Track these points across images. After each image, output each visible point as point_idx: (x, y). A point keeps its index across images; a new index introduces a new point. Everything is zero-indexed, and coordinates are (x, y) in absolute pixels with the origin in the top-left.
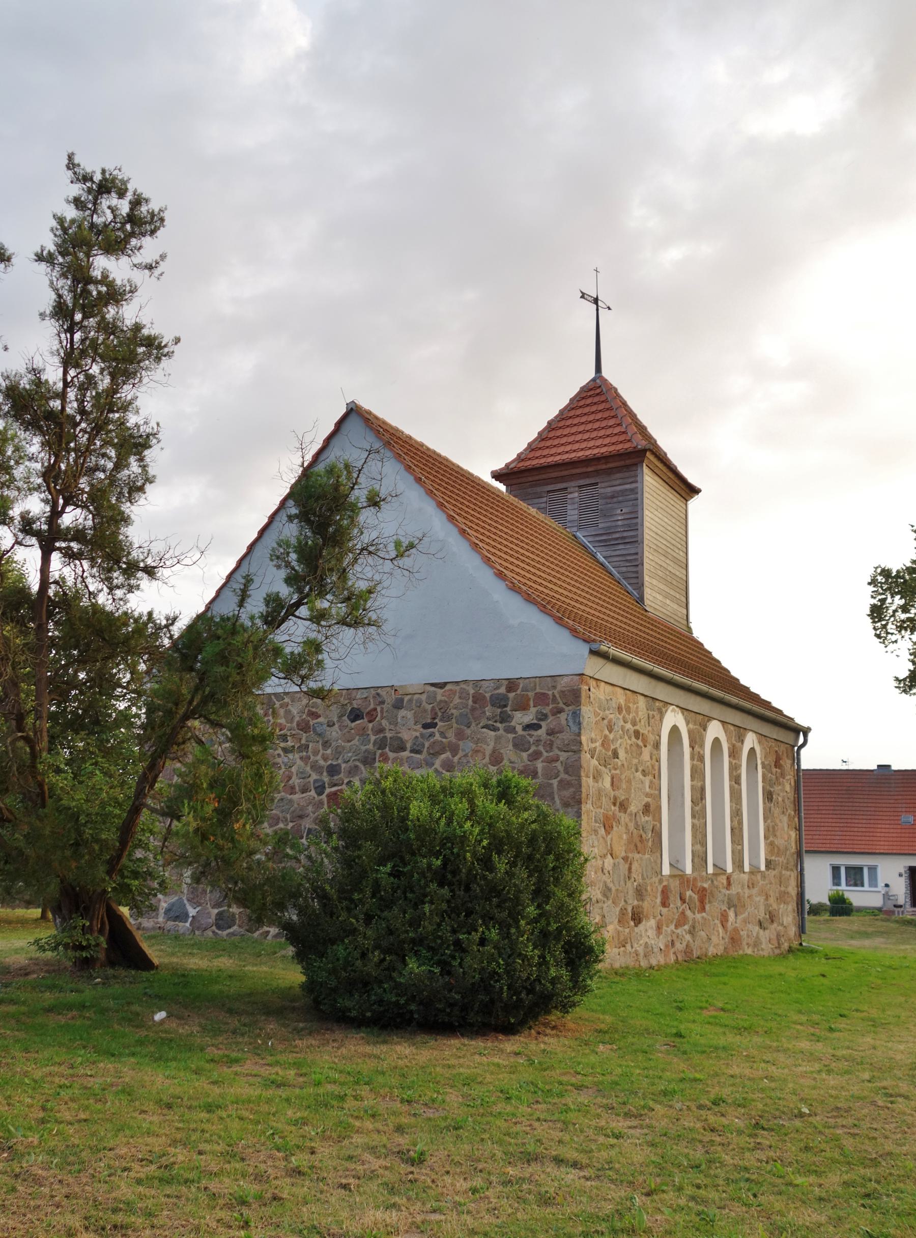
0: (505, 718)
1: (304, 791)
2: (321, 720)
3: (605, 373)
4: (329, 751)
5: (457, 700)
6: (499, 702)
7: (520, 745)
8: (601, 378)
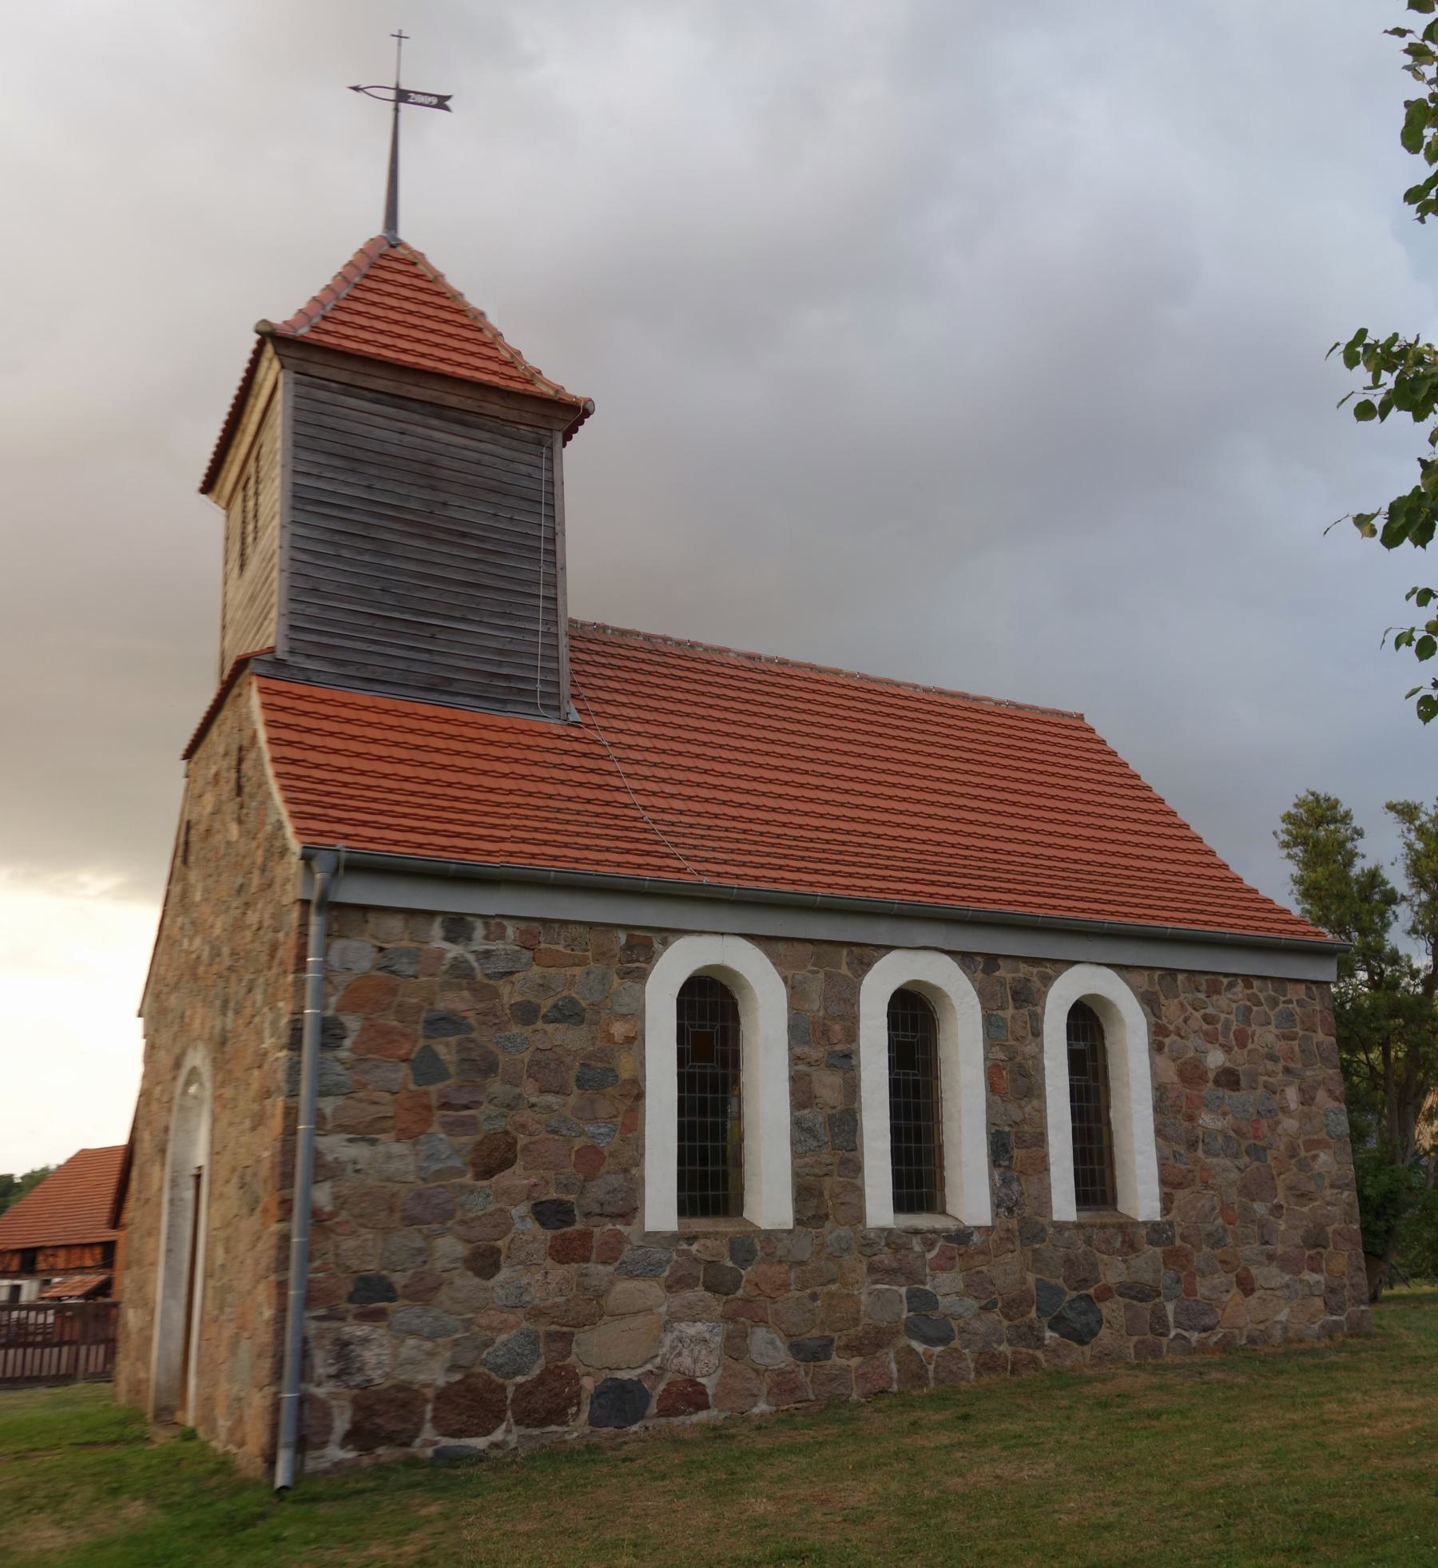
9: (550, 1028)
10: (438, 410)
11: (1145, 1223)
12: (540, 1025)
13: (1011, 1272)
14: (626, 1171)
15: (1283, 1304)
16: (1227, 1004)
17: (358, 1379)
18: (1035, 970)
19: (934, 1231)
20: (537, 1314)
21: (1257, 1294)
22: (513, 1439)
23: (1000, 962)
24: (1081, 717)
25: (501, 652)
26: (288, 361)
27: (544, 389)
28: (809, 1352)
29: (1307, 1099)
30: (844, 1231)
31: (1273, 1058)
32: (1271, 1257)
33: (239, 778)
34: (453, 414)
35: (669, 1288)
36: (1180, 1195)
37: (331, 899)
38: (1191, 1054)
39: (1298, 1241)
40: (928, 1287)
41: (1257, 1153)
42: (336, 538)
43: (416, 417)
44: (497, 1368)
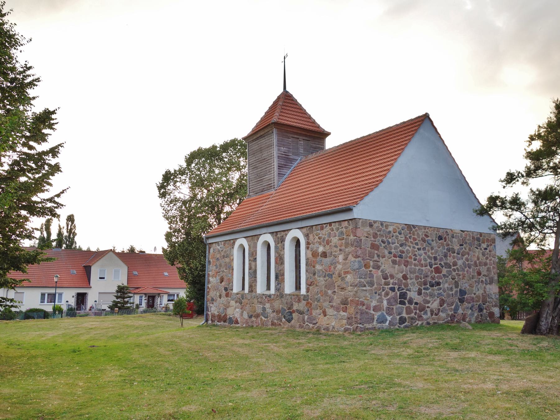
0: (480, 245)
1: (426, 266)
2: (429, 238)
3: (287, 89)
4: (433, 251)
5: (468, 238)
6: (478, 240)
7: (483, 254)
8: (287, 92)
13: (278, 305)
28: (250, 317)
30: (254, 294)
32: (332, 306)
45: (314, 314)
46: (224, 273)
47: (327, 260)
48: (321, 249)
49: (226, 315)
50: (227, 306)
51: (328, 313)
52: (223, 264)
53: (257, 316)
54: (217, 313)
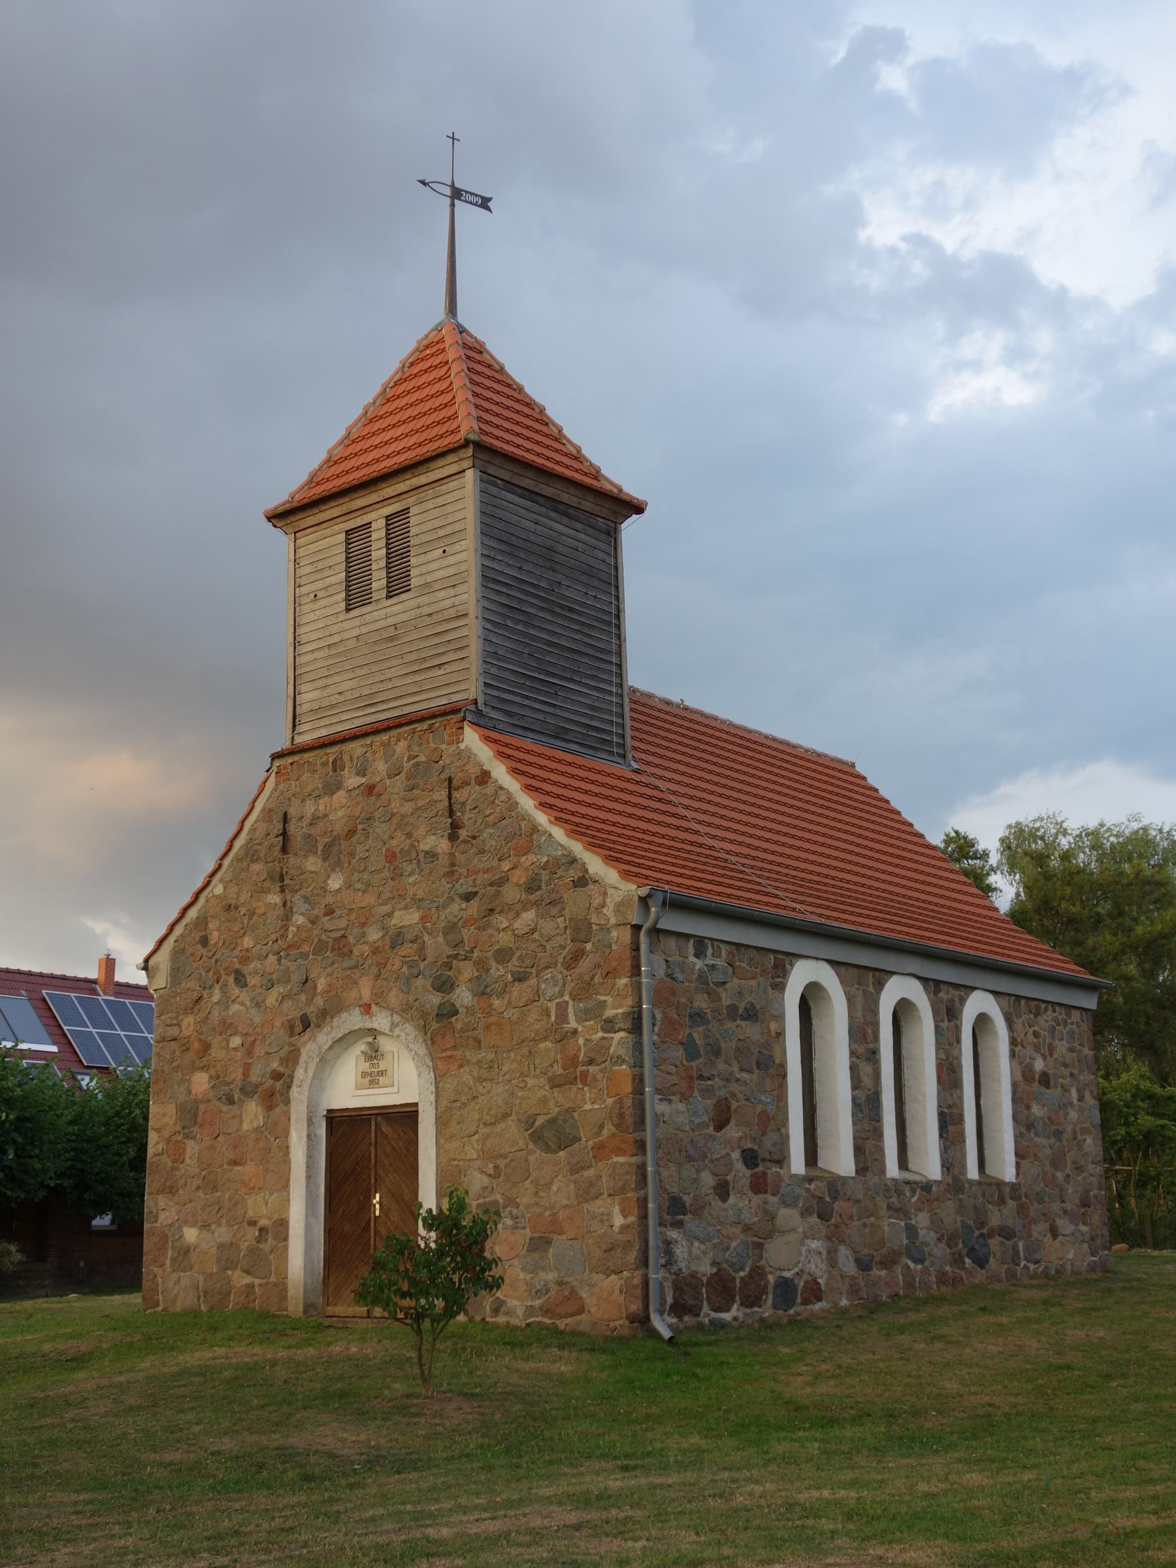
9: (744, 1023)
10: (554, 504)
11: (1008, 1183)
12: (739, 1022)
13: (949, 1214)
14: (779, 1130)
15: (1069, 1249)
16: (1046, 1020)
17: (675, 1268)
18: (957, 993)
19: (916, 1183)
20: (747, 1229)
21: (1060, 1238)
22: (740, 1315)
23: (941, 986)
24: (853, 765)
25: (591, 707)
26: (478, 462)
27: (609, 487)
28: (864, 1265)
29: (1081, 1099)
30: (876, 1179)
31: (1065, 1065)
32: (1065, 1212)
33: (450, 804)
34: (562, 507)
35: (802, 1215)
36: (1024, 1163)
37: (658, 926)
38: (1028, 1060)
39: (1077, 1201)
40: (913, 1222)
41: (1058, 1134)
42: (504, 611)
43: (543, 510)
44: (732, 1265)
45: (1035, 1234)
46: (734, 1087)
47: (1053, 1093)
48: (1039, 1065)
49: (758, 1272)
50: (760, 1235)
51: (1061, 1230)
52: (728, 1046)
53: (888, 1262)
54: (706, 1269)
